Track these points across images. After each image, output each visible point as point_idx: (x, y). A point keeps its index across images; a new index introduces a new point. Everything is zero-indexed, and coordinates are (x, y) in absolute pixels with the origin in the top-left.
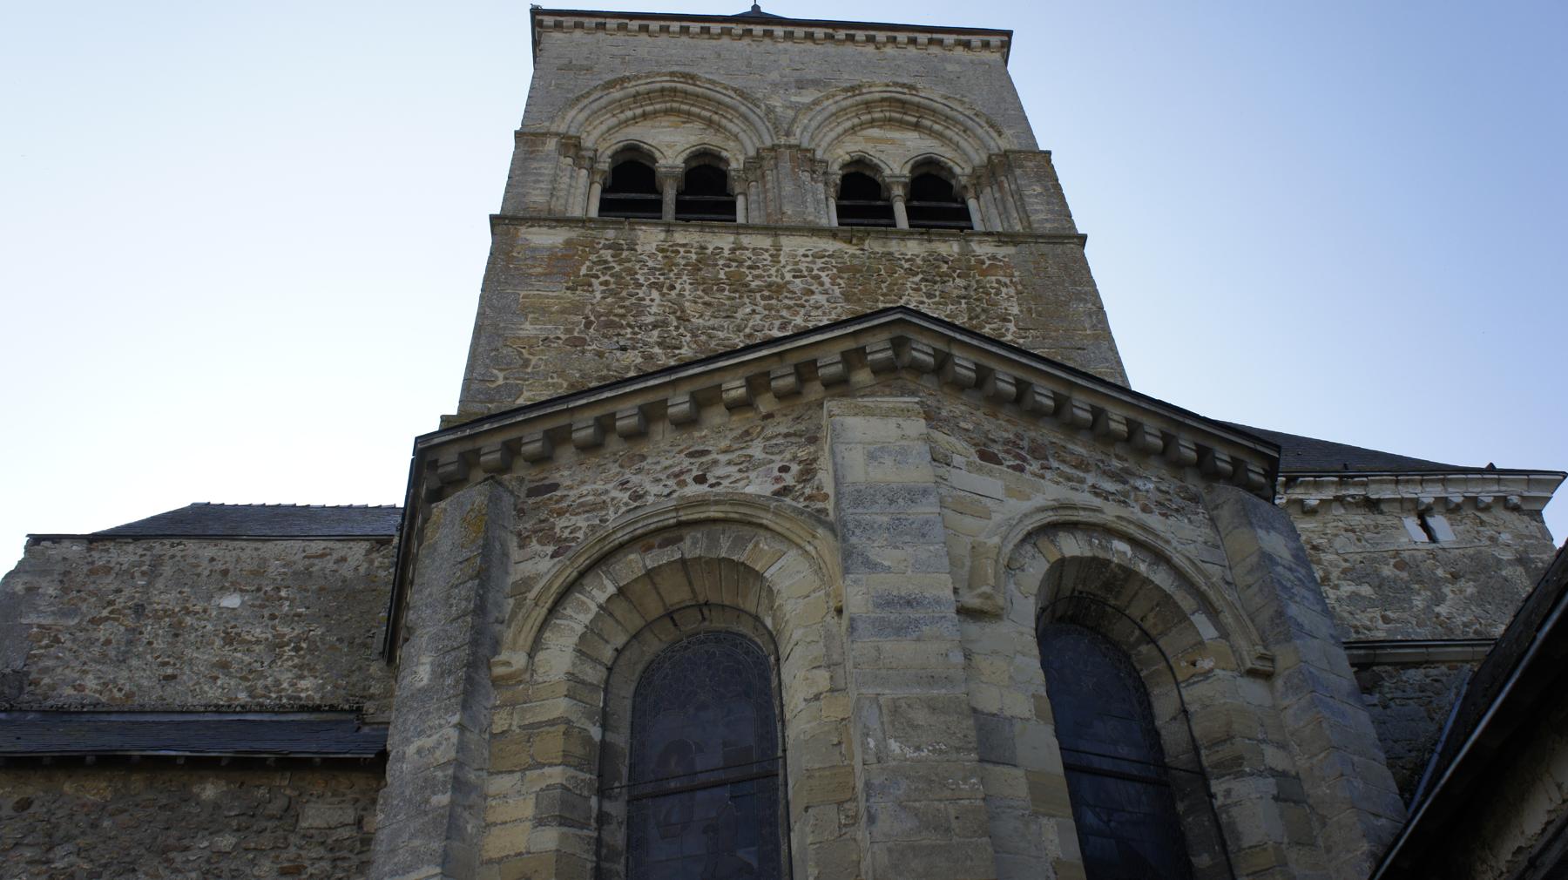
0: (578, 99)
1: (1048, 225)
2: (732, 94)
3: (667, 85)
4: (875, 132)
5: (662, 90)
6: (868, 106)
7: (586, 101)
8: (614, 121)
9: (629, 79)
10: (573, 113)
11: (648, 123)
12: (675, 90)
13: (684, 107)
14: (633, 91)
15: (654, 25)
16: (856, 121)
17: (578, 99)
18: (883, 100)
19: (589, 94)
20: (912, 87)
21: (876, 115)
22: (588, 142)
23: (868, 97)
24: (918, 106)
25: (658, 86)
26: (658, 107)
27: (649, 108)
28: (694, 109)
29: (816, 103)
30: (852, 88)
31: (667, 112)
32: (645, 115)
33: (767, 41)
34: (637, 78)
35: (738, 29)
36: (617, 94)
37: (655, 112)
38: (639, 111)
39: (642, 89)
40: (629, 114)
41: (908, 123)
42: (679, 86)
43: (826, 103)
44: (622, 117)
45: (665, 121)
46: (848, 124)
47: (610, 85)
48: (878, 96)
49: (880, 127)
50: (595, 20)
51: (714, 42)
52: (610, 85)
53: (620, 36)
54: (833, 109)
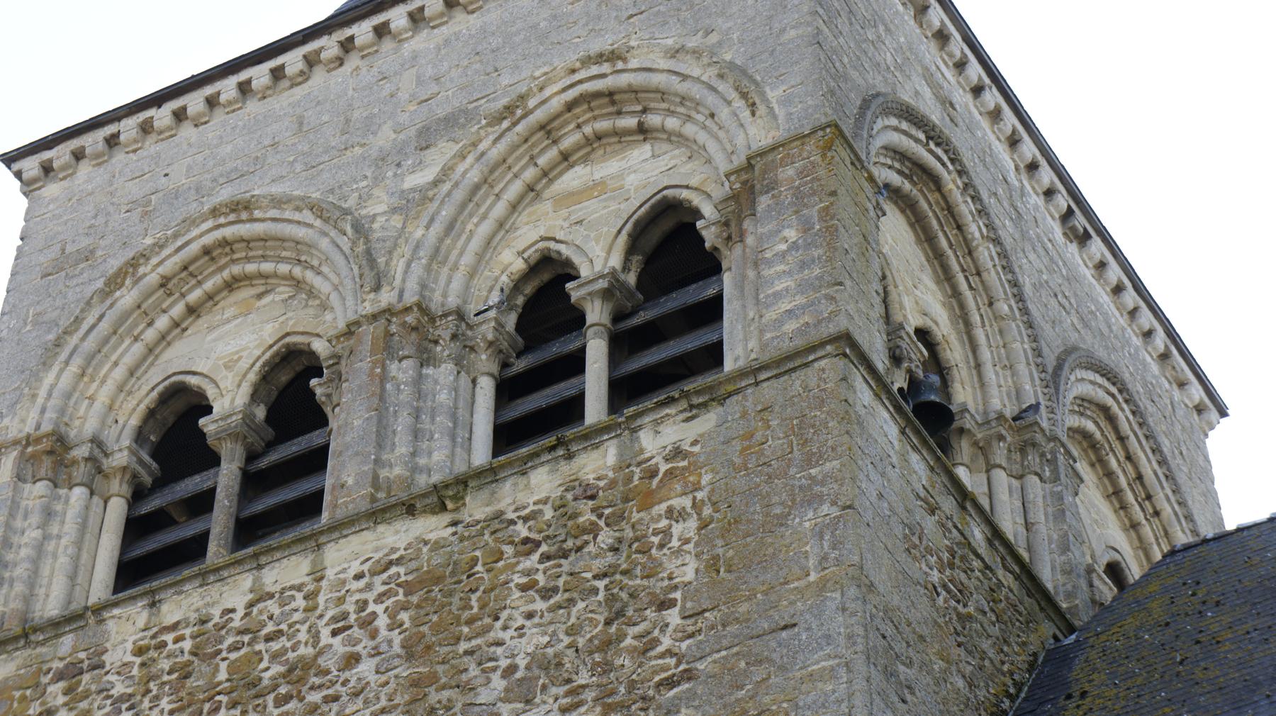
0: (58, 344)
1: (791, 326)
2: (307, 216)
3: (208, 240)
4: (574, 178)
5: (207, 251)
6: (545, 128)
7: (74, 340)
8: (138, 349)
9: (144, 256)
10: (49, 378)
11: (203, 323)
12: (224, 243)
13: (251, 268)
14: (153, 279)
15: (194, 102)
16: (530, 174)
17: (58, 344)
18: (570, 106)
19: (78, 321)
20: (612, 56)
21: (566, 143)
22: (86, 423)
23: (540, 115)
24: (633, 91)
25: (195, 248)
26: (209, 285)
27: (194, 296)
28: (267, 267)
29: (446, 172)
30: (509, 109)
31: (231, 285)
32: (193, 311)
33: (387, 45)
34: (160, 246)
35: (329, 45)
36: (127, 298)
37: (210, 297)
38: (178, 310)
39: (169, 267)
40: (162, 322)
41: (627, 132)
42: (228, 232)
43: (461, 168)
44: (150, 335)
45: (229, 306)
46: (516, 188)
47: (115, 282)
48: (556, 104)
49: (585, 160)
50: (232, 82)
51: (298, 92)
52: (115, 282)
53: (151, 146)
54: (474, 176)
